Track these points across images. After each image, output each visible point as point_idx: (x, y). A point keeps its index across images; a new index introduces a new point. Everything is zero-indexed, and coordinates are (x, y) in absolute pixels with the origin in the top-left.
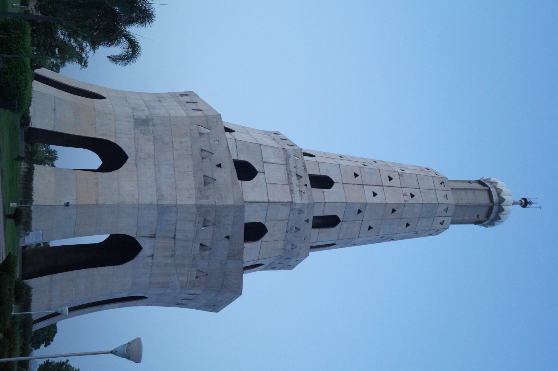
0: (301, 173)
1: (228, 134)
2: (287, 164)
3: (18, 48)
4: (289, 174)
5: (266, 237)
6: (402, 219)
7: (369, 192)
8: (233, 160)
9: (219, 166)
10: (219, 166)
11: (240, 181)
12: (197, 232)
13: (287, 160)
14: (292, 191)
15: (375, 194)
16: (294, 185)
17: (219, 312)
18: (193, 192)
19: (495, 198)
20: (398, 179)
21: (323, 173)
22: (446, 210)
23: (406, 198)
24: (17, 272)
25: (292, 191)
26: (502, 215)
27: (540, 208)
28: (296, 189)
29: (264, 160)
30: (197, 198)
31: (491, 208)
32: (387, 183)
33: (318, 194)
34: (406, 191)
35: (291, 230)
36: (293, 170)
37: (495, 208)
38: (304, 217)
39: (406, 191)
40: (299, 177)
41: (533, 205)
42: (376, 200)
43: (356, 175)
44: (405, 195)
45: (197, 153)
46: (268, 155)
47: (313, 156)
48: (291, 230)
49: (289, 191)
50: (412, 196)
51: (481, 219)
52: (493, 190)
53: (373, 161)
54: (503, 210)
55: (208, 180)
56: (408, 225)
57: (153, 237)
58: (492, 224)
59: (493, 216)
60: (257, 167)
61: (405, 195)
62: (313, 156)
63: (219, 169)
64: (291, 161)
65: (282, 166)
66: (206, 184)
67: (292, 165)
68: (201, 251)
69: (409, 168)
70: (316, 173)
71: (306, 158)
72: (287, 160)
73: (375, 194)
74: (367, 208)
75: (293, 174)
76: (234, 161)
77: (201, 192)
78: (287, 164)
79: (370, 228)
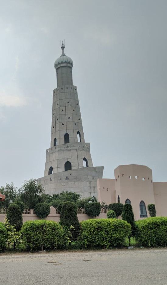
2: (64, 150)
3: (45, 241)
4: (67, 150)
7: (68, 120)
8: (49, 175)
9: (71, 174)
10: (71, 174)
13: (62, 150)
16: (71, 149)
17: (118, 166)
19: (65, 65)
24: (104, 220)
26: (67, 61)
27: (64, 40)
28: (72, 148)
29: (63, 158)
32: (64, 111)
34: (66, 105)
41: (64, 43)
43: (63, 124)
45: (67, 181)
46: (61, 156)
50: (68, 103)
54: (69, 62)
57: (90, 193)
63: (72, 175)
67: (64, 149)
70: (63, 139)
72: (62, 150)
73: (69, 118)
74: (74, 121)
75: (67, 149)
76: (50, 174)
77: (79, 180)
78: (64, 150)
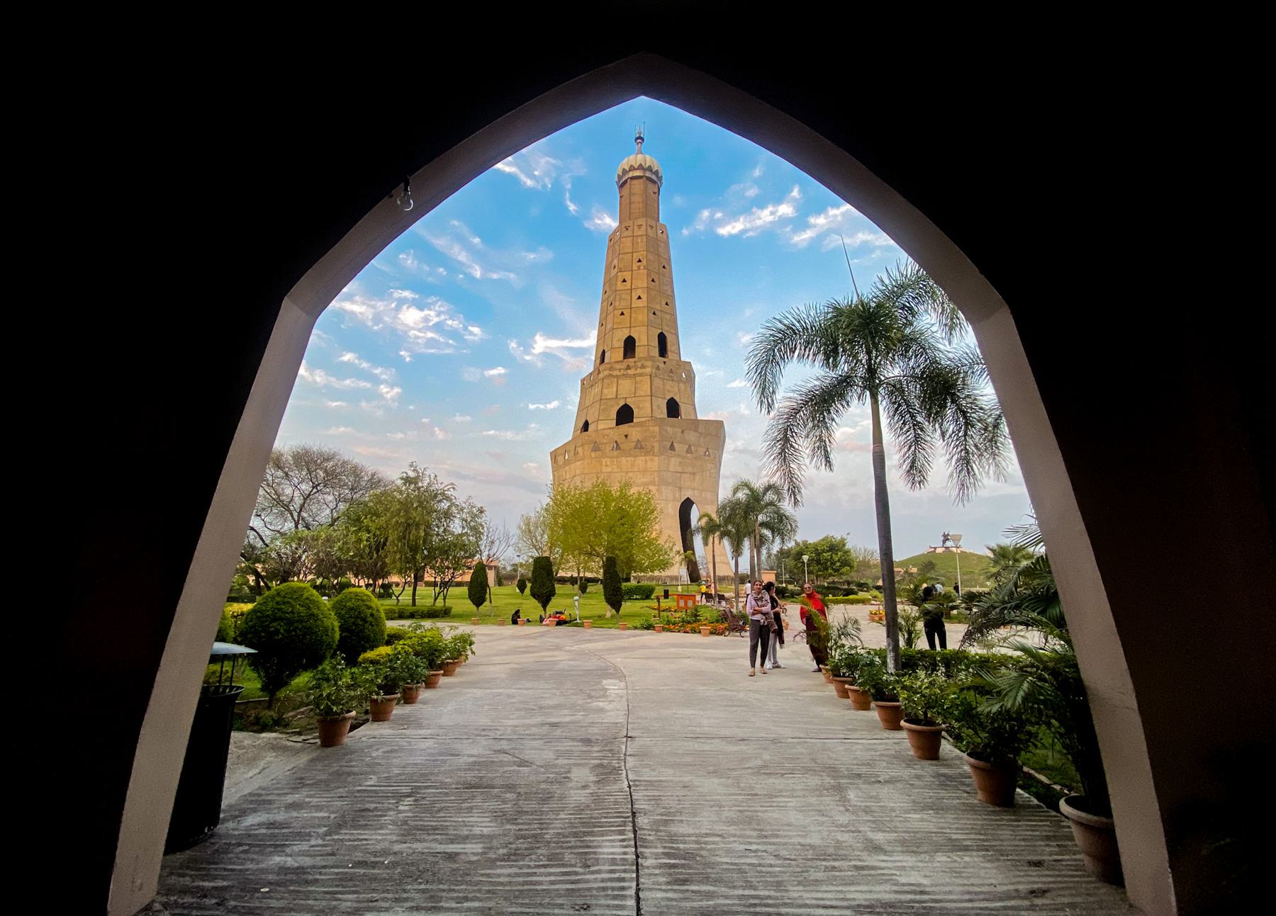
0: (624, 365)
1: (591, 428)
2: (617, 377)
4: (626, 376)
5: (677, 399)
6: (631, 251)
9: (626, 436)
10: (626, 436)
11: (635, 420)
12: (679, 456)
14: (641, 375)
15: (639, 298)
18: (648, 458)
20: (625, 273)
21: (622, 344)
22: (652, 227)
23: (642, 268)
25: (641, 375)
28: (639, 371)
30: (653, 455)
31: (649, 179)
32: (628, 284)
33: (640, 351)
34: (635, 267)
35: (671, 377)
36: (622, 372)
37: (648, 174)
38: (662, 365)
39: (635, 267)
40: (628, 368)
42: (644, 297)
43: (622, 314)
44: (639, 267)
45: (615, 453)
47: (604, 352)
48: (671, 377)
49: (641, 378)
50: (640, 261)
51: (656, 190)
52: (631, 174)
53: (988, 548)
55: (640, 447)
56: (664, 267)
58: (660, 178)
59: (654, 177)
60: (622, 403)
61: (639, 267)
62: (604, 352)
64: (615, 373)
65: (620, 382)
66: (642, 448)
68: (692, 453)
69: (610, 259)
71: (606, 360)
73: (639, 298)
79: (667, 304)
